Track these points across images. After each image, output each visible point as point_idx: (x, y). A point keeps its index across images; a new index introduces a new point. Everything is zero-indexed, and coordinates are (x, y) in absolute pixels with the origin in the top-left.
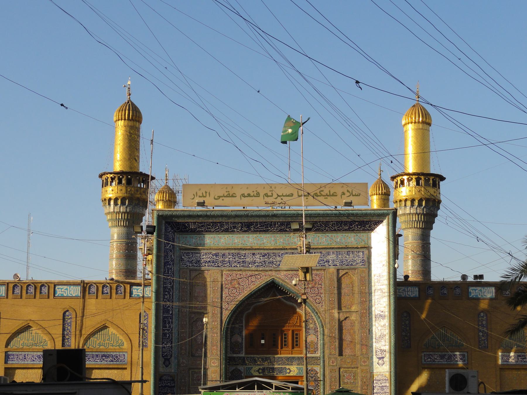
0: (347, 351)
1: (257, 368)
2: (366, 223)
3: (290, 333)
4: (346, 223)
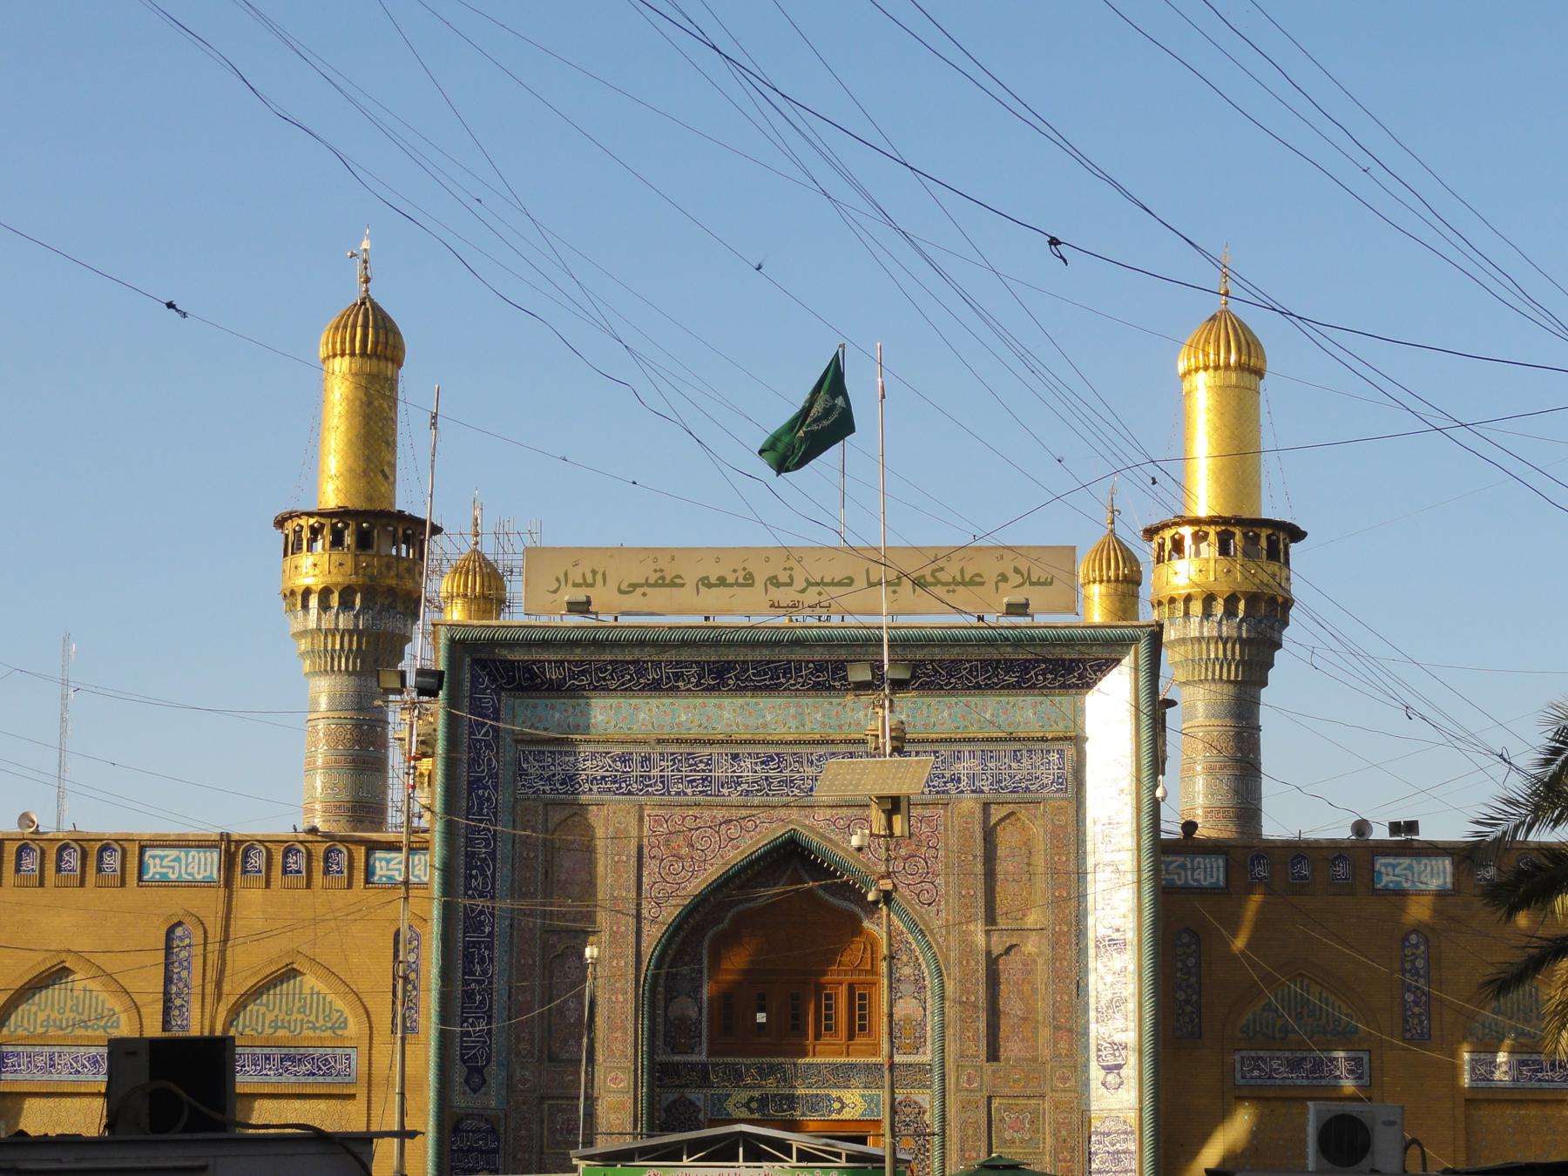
0: (1011, 1048)
1: (744, 1095)
2: (1068, 665)
4: (1010, 665)
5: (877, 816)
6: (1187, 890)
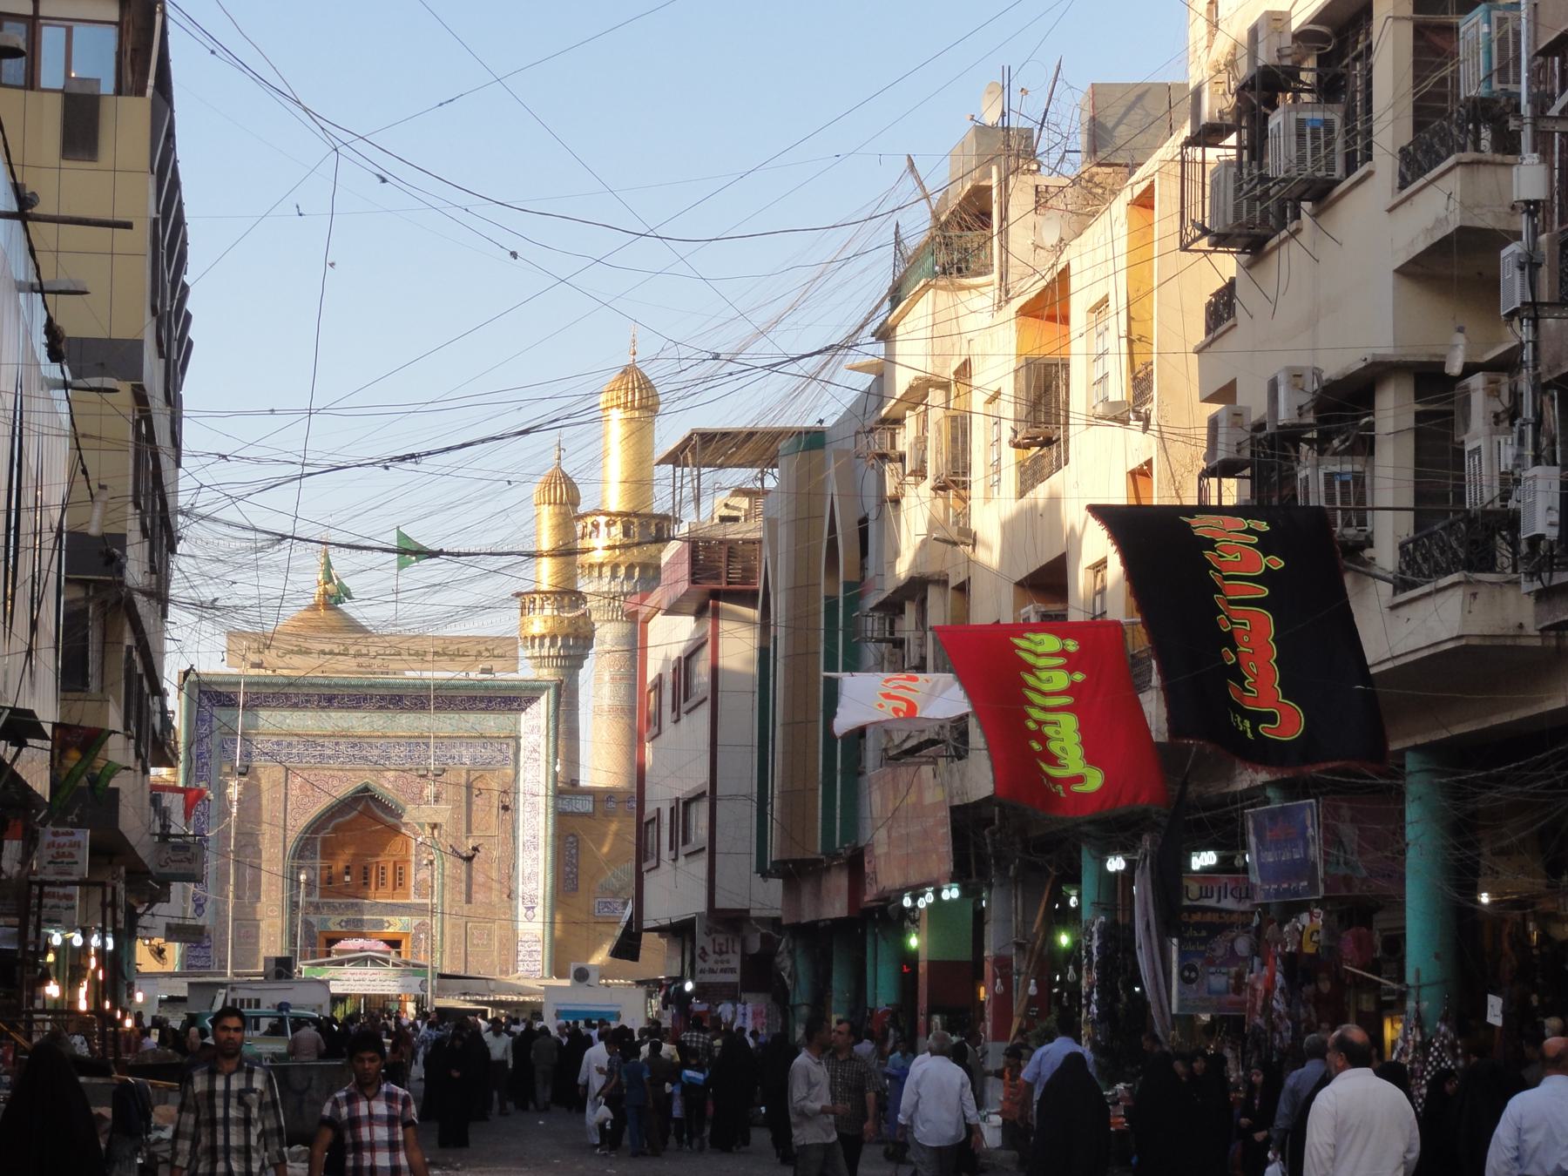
0: (478, 896)
1: (338, 919)
2: (513, 699)
3: (391, 866)
4: (482, 699)
5: (428, 830)
6: (573, 814)
